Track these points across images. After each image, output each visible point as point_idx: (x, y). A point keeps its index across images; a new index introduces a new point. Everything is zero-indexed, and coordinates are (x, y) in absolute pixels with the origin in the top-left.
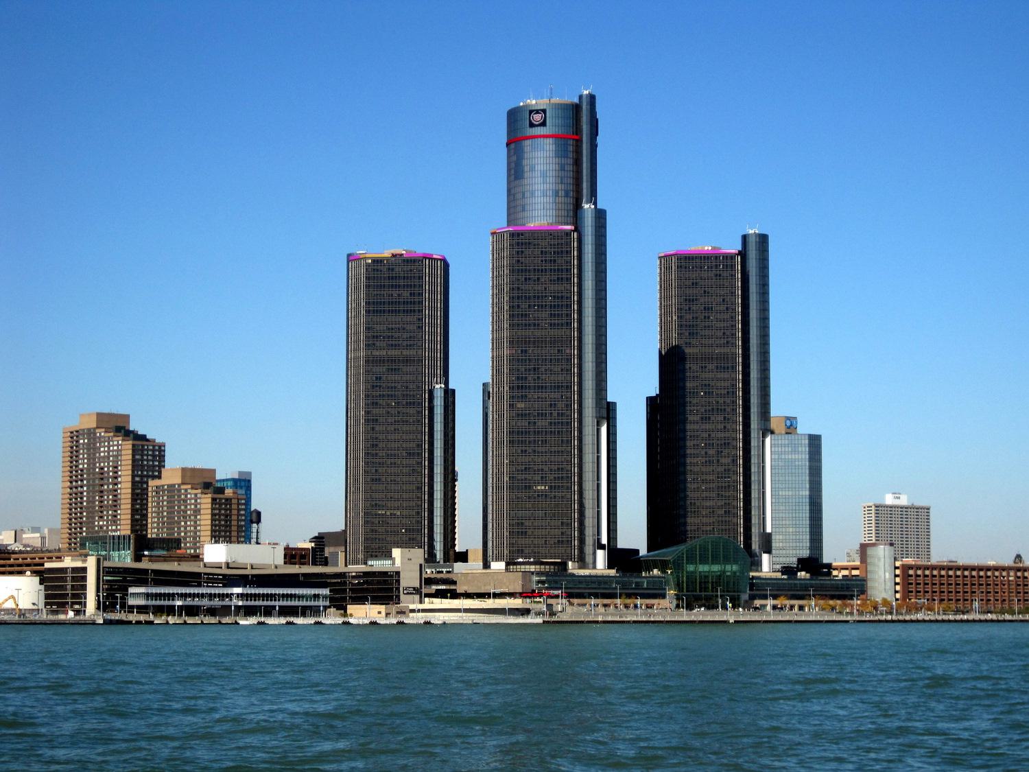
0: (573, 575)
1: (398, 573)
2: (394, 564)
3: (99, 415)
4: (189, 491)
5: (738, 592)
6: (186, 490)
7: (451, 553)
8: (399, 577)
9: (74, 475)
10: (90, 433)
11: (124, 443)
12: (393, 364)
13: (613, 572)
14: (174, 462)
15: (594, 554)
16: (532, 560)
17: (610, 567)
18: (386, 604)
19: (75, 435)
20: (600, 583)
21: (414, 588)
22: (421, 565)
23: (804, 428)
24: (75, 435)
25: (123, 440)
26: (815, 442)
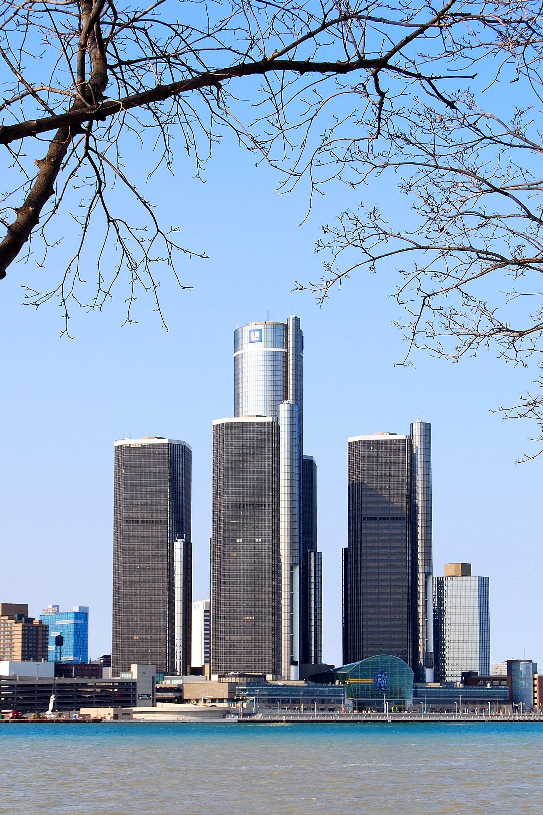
0: (270, 685)
1: (134, 684)
2: (132, 676)
4: (13, 625)
5: (404, 698)
6: (4, 620)
7: (188, 669)
8: (136, 686)
13: (302, 683)
15: (289, 669)
16: (238, 673)
17: (301, 679)
18: (115, 708)
20: (292, 691)
21: (148, 696)
22: (153, 678)
23: (476, 572)
26: (484, 583)
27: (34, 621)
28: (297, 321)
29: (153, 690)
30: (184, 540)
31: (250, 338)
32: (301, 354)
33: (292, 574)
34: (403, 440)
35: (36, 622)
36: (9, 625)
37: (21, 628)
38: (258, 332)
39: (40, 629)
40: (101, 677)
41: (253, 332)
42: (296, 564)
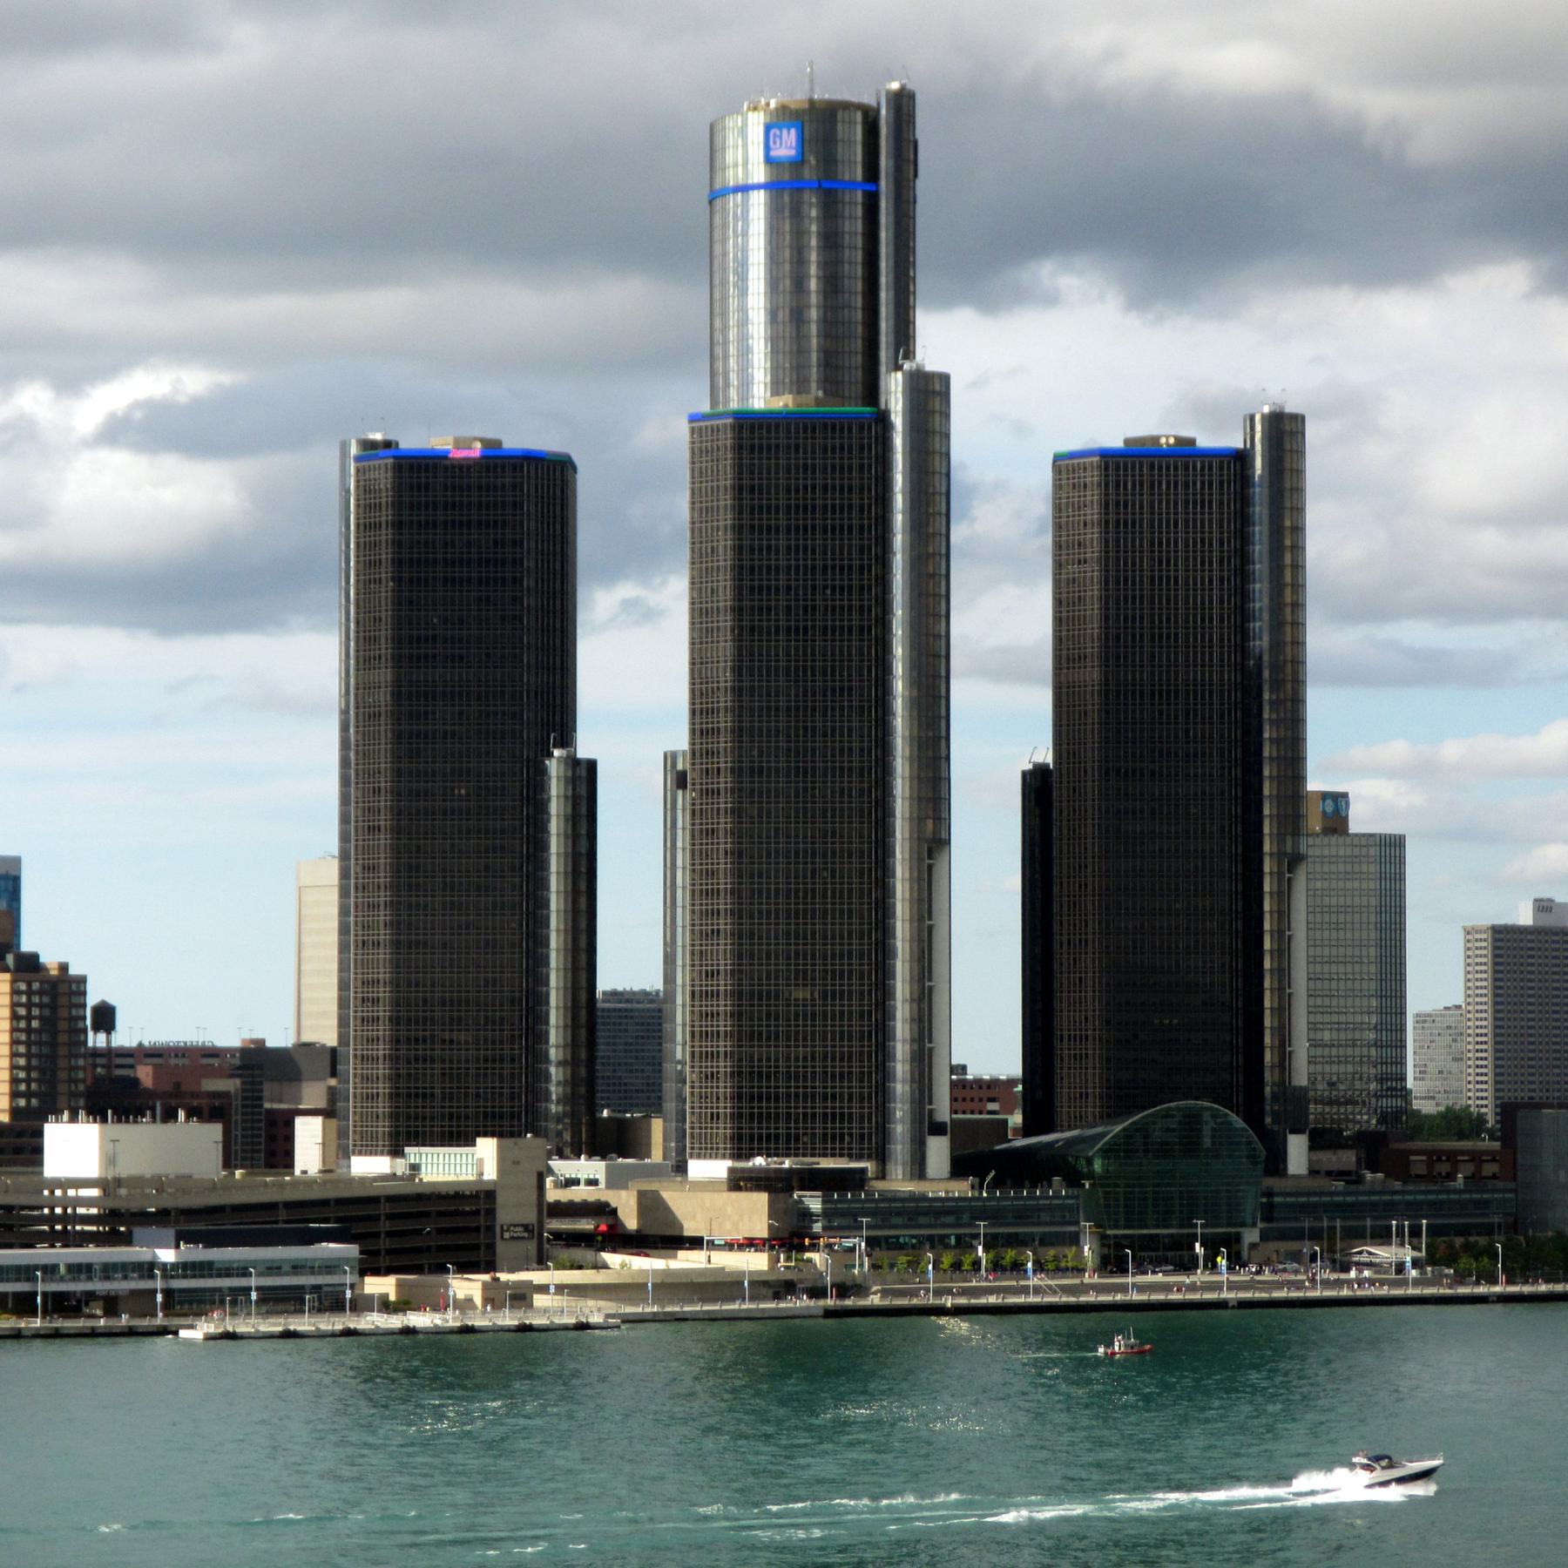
13: (962, 1188)
21: (526, 1227)
29: (540, 1212)
39: (62, 988)
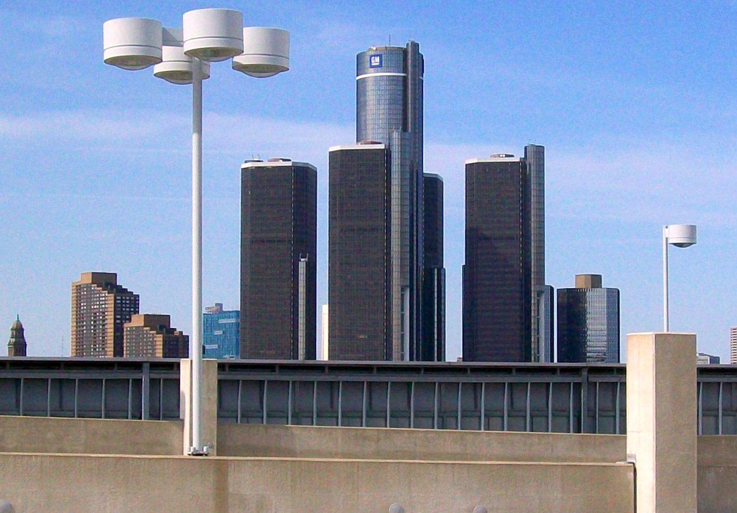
3: (94, 274)
6: (146, 330)
9: (79, 318)
10: (88, 286)
11: (109, 295)
12: (540, 253)
14: (146, 308)
19: (79, 288)
23: (605, 284)
24: (79, 288)
25: (108, 293)
27: (175, 332)
28: (415, 46)
30: (307, 260)
31: (371, 63)
32: (421, 78)
33: (402, 295)
34: (517, 162)
35: (176, 333)
36: (151, 336)
37: (161, 339)
38: (378, 58)
39: (180, 340)
40: (26, 355)
41: (373, 58)
42: (407, 286)
